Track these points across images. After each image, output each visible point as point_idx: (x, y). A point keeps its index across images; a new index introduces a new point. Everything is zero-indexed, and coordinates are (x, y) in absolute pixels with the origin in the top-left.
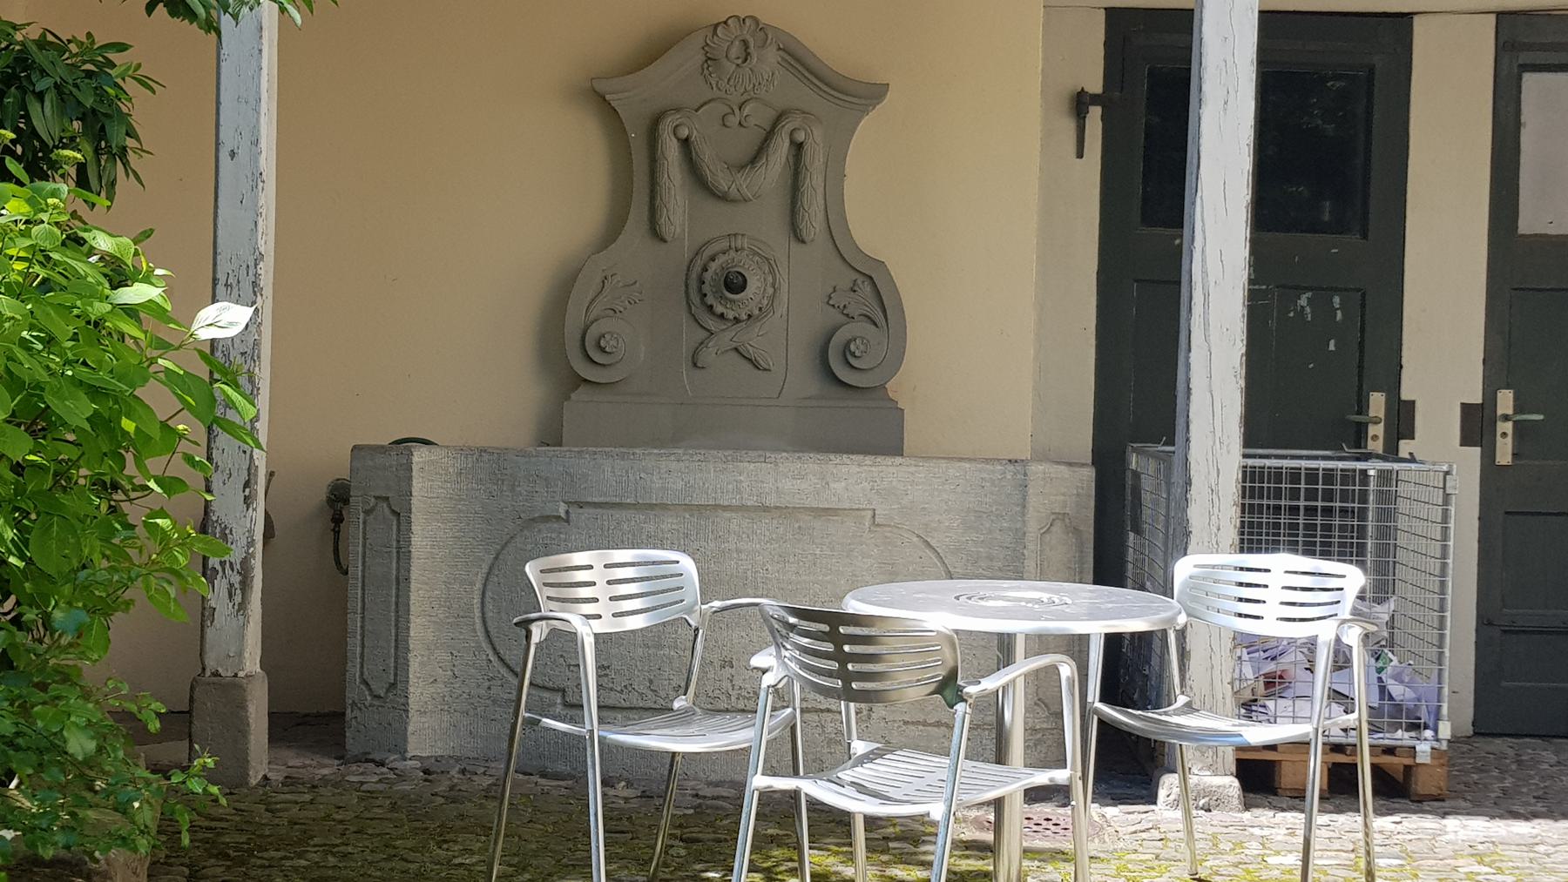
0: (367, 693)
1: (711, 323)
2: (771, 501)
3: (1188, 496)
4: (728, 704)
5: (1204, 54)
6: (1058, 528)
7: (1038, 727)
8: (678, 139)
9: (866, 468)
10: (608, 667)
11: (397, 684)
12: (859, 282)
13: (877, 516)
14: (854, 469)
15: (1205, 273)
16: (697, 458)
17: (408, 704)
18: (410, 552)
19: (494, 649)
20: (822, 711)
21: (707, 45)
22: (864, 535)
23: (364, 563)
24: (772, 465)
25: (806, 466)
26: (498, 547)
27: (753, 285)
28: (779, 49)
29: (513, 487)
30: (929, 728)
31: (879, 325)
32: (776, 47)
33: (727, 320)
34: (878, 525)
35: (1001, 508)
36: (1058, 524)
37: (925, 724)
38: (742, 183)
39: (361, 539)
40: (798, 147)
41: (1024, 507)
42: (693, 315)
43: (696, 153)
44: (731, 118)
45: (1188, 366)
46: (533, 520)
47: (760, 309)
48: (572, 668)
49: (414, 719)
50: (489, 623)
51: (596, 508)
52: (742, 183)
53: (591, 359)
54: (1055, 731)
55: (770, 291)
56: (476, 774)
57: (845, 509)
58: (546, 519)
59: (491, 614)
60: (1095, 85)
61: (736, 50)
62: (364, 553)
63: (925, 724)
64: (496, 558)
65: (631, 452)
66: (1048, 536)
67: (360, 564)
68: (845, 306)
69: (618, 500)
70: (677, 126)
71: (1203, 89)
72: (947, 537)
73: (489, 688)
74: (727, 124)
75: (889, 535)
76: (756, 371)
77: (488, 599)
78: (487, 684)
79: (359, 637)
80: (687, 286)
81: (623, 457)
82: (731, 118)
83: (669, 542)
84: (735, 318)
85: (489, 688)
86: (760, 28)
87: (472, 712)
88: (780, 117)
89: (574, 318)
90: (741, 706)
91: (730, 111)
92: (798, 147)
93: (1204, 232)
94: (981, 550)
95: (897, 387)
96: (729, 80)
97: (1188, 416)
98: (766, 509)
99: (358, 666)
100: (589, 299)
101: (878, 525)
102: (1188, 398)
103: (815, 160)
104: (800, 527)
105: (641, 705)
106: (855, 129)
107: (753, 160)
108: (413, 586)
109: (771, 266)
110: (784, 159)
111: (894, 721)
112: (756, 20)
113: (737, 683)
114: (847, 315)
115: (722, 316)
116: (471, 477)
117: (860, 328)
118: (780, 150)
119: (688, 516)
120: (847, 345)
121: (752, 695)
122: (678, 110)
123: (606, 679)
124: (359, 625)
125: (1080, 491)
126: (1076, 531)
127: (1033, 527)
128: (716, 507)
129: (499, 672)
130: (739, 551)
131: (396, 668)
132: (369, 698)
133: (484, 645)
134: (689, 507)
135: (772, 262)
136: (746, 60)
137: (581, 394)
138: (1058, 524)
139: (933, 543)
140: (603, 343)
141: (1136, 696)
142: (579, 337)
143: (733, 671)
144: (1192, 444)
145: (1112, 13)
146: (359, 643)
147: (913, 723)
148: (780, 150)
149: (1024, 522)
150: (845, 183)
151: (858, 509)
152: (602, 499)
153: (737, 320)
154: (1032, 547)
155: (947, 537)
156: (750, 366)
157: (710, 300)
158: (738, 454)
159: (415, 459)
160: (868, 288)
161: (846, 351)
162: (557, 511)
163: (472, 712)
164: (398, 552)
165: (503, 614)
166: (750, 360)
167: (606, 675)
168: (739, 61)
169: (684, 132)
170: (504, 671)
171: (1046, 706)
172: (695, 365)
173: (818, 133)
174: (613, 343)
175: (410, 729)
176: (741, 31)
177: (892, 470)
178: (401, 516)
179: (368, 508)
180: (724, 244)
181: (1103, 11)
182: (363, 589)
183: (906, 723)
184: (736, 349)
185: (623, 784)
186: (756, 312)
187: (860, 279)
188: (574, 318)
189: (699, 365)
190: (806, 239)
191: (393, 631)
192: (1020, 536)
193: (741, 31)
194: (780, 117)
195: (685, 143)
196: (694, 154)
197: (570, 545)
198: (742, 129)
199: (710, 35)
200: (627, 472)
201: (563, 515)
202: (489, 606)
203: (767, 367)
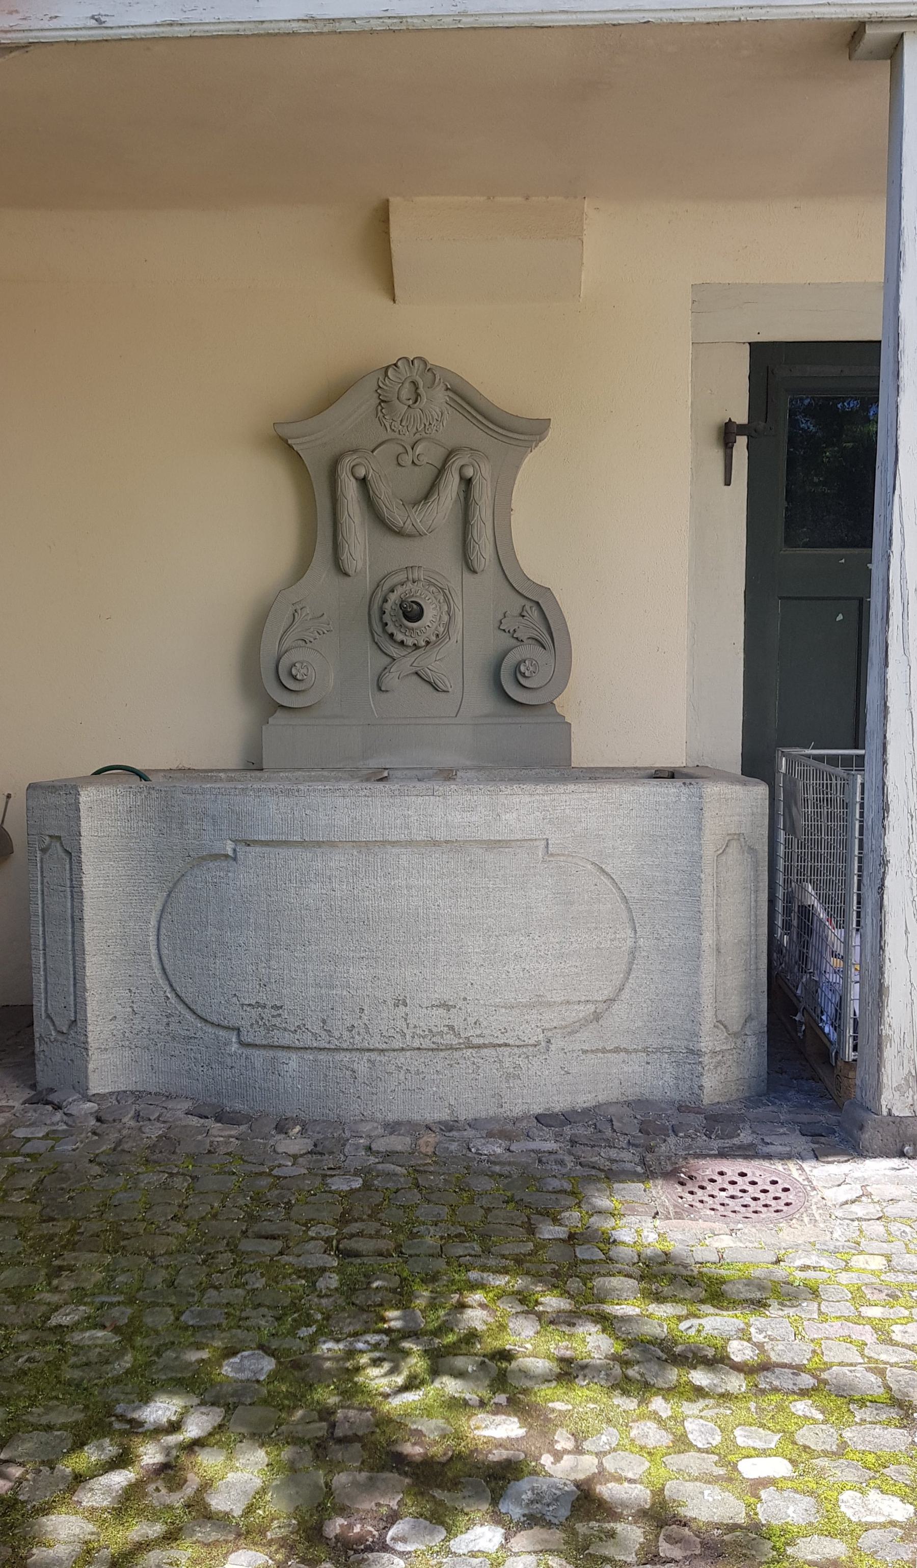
0: (52, 1028)
1: (394, 651)
2: (441, 835)
3: (886, 822)
4: (404, 1043)
5: (901, 332)
6: (734, 849)
7: (718, 1049)
8: (356, 479)
9: (537, 797)
10: (281, 1007)
11: (77, 1022)
12: (527, 608)
13: (550, 846)
14: (527, 799)
15: (903, 578)
16: (362, 793)
17: (87, 1042)
18: (82, 892)
19: (171, 986)
20: (500, 1046)
21: (380, 387)
22: (538, 866)
23: (43, 901)
24: (441, 798)
25: (475, 797)
26: (171, 885)
27: (430, 614)
28: (447, 389)
29: (181, 826)
30: (609, 1055)
31: (547, 647)
32: (444, 387)
33: (407, 646)
34: (552, 855)
35: (677, 831)
36: (734, 844)
37: (604, 1051)
38: (418, 518)
39: (39, 877)
40: (467, 483)
41: (700, 829)
42: (376, 643)
43: (374, 492)
44: (405, 457)
45: (884, 683)
46: (203, 858)
47: (437, 635)
48: (245, 1007)
49: (94, 1057)
50: (165, 959)
51: (262, 846)
52: (418, 518)
53: (286, 687)
54: (734, 1051)
55: (446, 618)
56: (150, 1120)
57: (518, 840)
58: (215, 857)
59: (166, 952)
60: (741, 417)
61: (406, 392)
62: (43, 891)
63: (604, 1051)
64: (169, 896)
65: (295, 788)
66: (724, 858)
67: (40, 902)
68: (515, 631)
69: (284, 838)
70: (353, 467)
71: (901, 374)
72: (622, 862)
73: (168, 1024)
74: (403, 463)
75: (563, 864)
76: (435, 693)
77: (162, 937)
78: (165, 1020)
79: (42, 973)
80: (369, 615)
81: (288, 793)
82: (405, 457)
83: (337, 880)
84: (415, 645)
85: (168, 1024)
86: (428, 369)
87: (152, 1048)
88: (450, 454)
89: (269, 647)
90: (416, 1044)
91: (403, 451)
92: (467, 483)
93: (903, 535)
94: (657, 874)
95: (565, 704)
96: (401, 421)
97: (885, 737)
98: (435, 843)
99: (43, 1001)
100: (281, 632)
101: (552, 855)
102: (885, 717)
103: (484, 494)
104: (471, 862)
105: (315, 1045)
106: (521, 463)
107: (427, 497)
108: (87, 925)
109: (446, 596)
110: (454, 495)
111: (573, 1051)
112: (425, 362)
113: (412, 1021)
114: (517, 638)
115: (402, 643)
116: (140, 814)
117: (529, 651)
118: (451, 486)
119: (355, 853)
120: (518, 666)
121: (427, 1033)
122: (355, 451)
123: (279, 1019)
124: (42, 961)
125: (755, 810)
126: (751, 850)
127: (709, 852)
128: (384, 843)
129: (176, 1009)
130: (409, 887)
131: (75, 1005)
132: (53, 1033)
133: (161, 982)
134: (356, 844)
135: (447, 592)
136: (416, 401)
137: (279, 718)
138: (734, 844)
139: (608, 869)
140: (294, 672)
141: (799, 992)
142: (273, 666)
143: (407, 1009)
144: (890, 767)
145: (755, 348)
146: (42, 978)
147: (592, 1051)
148: (451, 486)
149: (700, 844)
150: (512, 517)
151: (531, 840)
152: (268, 838)
153: (416, 647)
154: (708, 869)
155: (622, 862)
156: (431, 689)
157: (391, 628)
158: (406, 788)
159: (83, 798)
160: (535, 613)
161: (516, 672)
162: (225, 849)
163: (152, 1048)
164: (71, 891)
165: (178, 953)
166: (430, 683)
167: (280, 1015)
168: (411, 402)
169: (361, 472)
170: (181, 1008)
171: (725, 1027)
172: (380, 689)
173: (486, 470)
174: (304, 671)
175: (91, 1066)
176: (411, 371)
177: (564, 797)
178: (73, 855)
179: (43, 846)
180: (402, 577)
181: (748, 346)
182: (44, 925)
183: (585, 1052)
184: (417, 673)
185: (298, 1128)
186: (434, 638)
187: (528, 605)
188: (269, 647)
189: (383, 689)
190: (477, 570)
191: (71, 969)
192: (696, 860)
193: (411, 371)
194: (450, 454)
195: (363, 482)
196: (371, 492)
197: (238, 883)
198: (416, 468)
199: (381, 379)
200: (292, 809)
201: (230, 853)
202: (164, 944)
203: (445, 689)
